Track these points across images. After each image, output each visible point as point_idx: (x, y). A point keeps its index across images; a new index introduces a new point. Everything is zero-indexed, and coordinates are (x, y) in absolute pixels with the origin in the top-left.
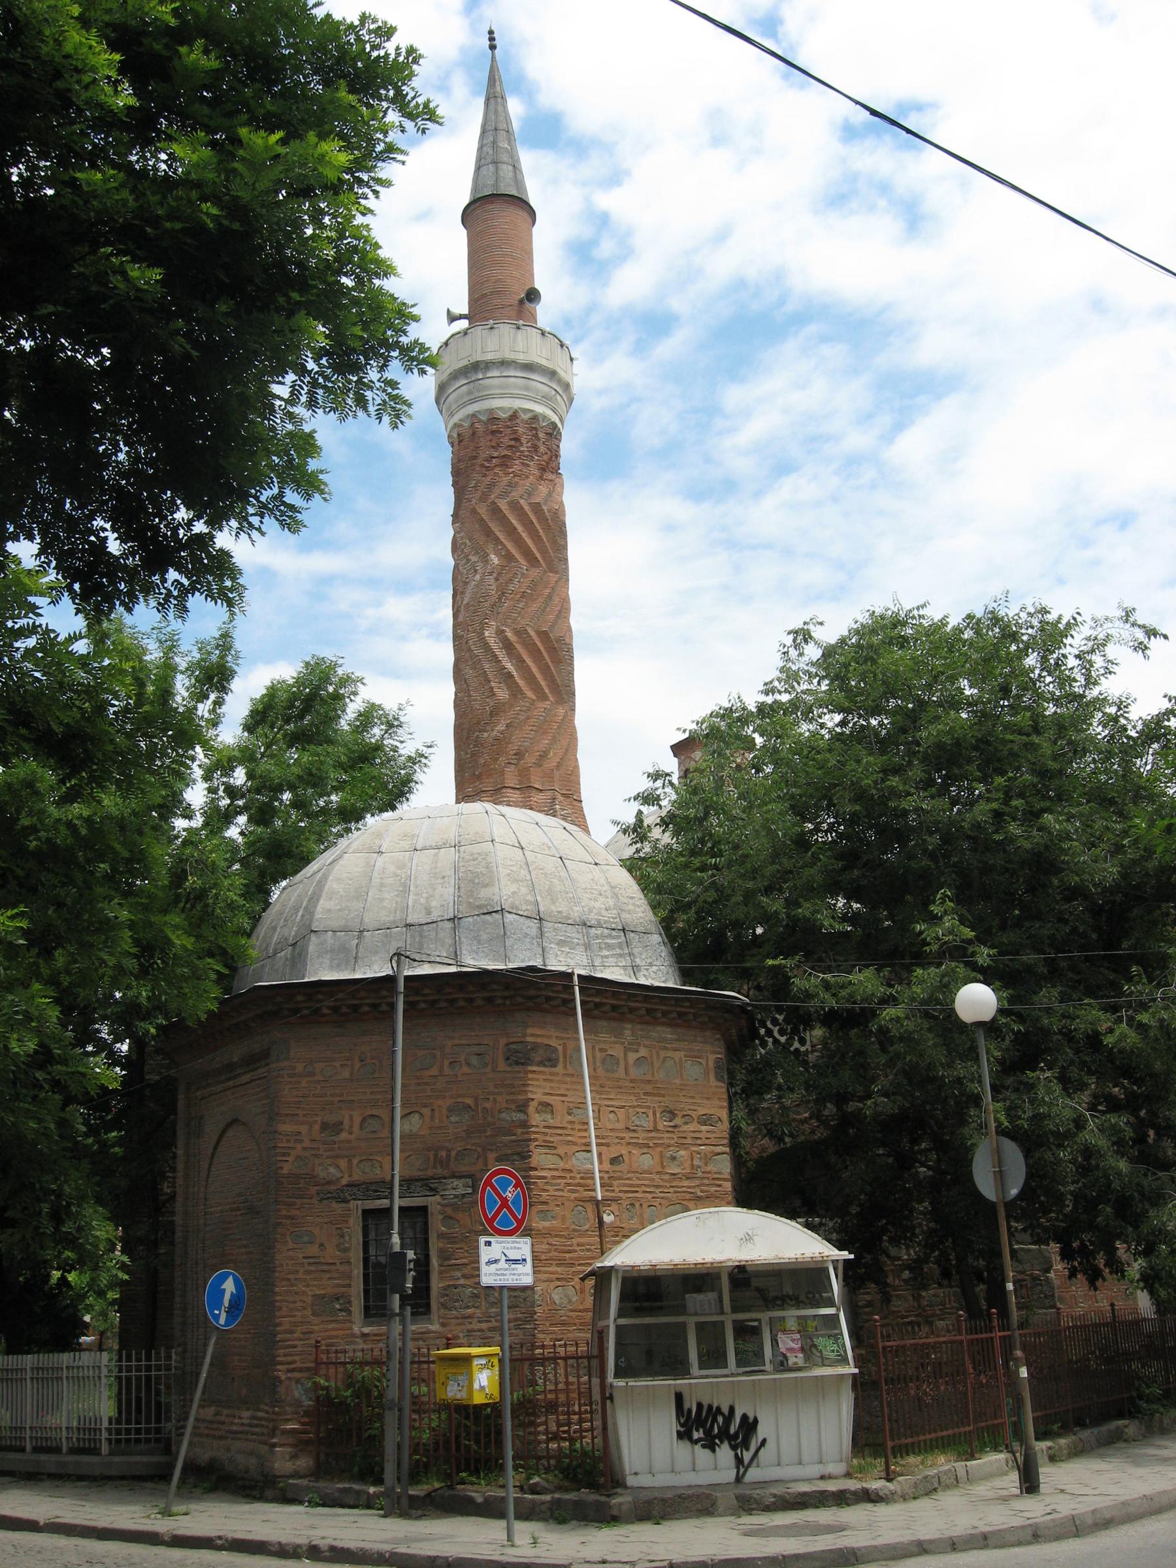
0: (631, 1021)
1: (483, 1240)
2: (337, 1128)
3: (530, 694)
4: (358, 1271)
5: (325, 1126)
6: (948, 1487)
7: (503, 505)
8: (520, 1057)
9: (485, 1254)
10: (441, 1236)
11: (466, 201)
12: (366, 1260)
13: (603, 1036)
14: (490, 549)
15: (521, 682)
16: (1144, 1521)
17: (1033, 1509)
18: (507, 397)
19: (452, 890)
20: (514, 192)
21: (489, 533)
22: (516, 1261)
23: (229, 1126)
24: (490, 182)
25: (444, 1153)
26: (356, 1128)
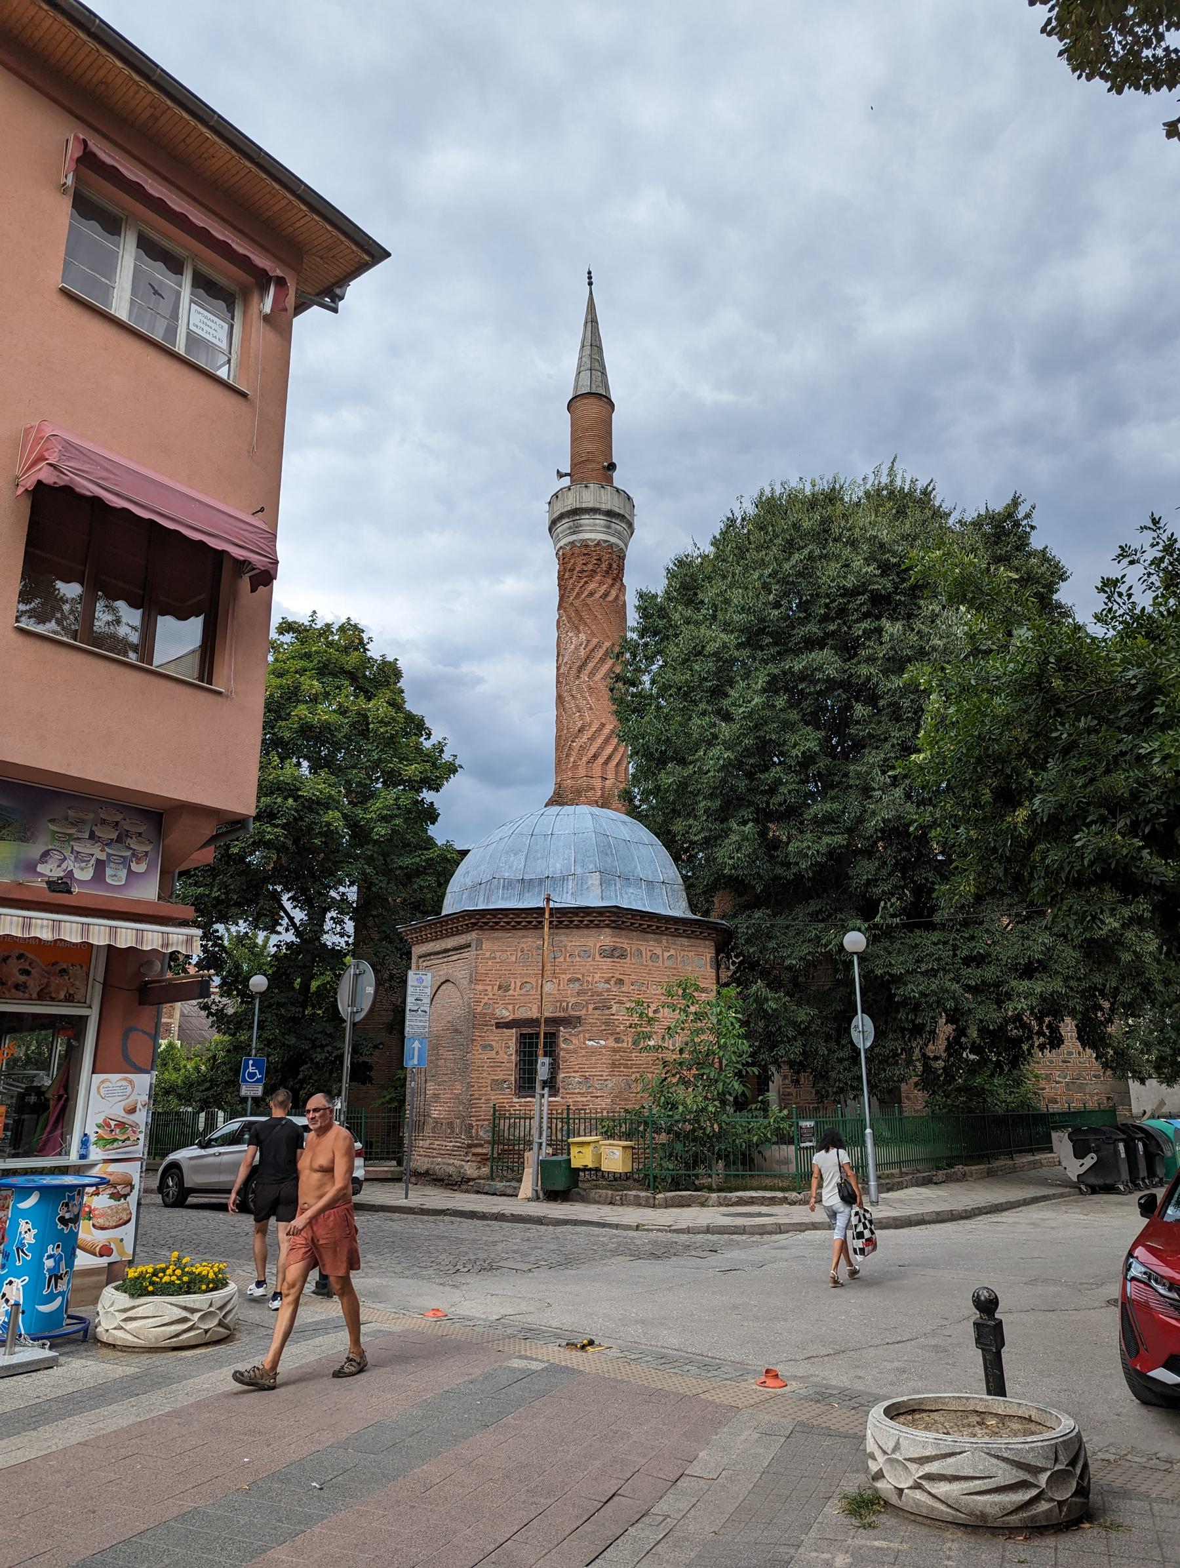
21: (581, 619)
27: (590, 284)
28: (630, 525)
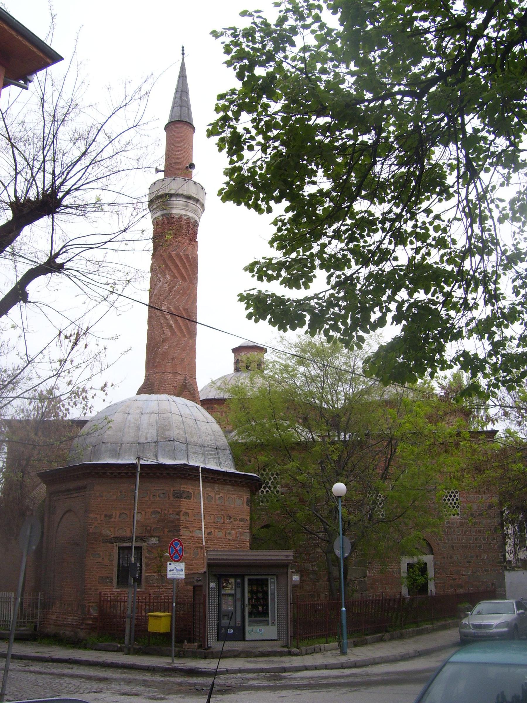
0: (218, 483)
1: (169, 563)
2: (110, 517)
3: (179, 334)
4: (116, 569)
5: (106, 516)
6: (317, 652)
7: (173, 253)
8: (179, 495)
9: (169, 568)
10: (146, 557)
11: (166, 122)
12: (119, 564)
13: (208, 489)
14: (167, 272)
15: (176, 329)
16: (379, 666)
17: (343, 659)
18: (178, 208)
19: (155, 431)
20: (187, 120)
21: (167, 266)
22: (179, 570)
23: (67, 512)
24: (178, 114)
25: (149, 528)
26: (117, 517)
27: (183, 54)
28: (203, 205)
